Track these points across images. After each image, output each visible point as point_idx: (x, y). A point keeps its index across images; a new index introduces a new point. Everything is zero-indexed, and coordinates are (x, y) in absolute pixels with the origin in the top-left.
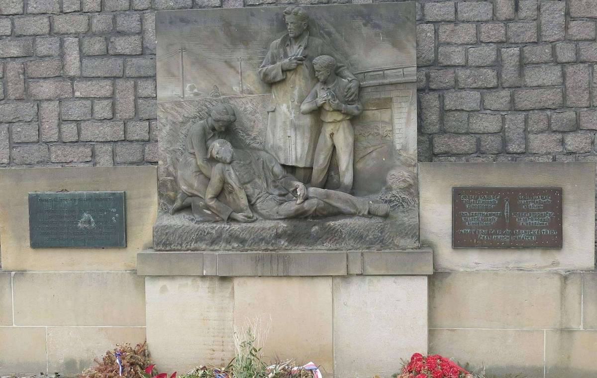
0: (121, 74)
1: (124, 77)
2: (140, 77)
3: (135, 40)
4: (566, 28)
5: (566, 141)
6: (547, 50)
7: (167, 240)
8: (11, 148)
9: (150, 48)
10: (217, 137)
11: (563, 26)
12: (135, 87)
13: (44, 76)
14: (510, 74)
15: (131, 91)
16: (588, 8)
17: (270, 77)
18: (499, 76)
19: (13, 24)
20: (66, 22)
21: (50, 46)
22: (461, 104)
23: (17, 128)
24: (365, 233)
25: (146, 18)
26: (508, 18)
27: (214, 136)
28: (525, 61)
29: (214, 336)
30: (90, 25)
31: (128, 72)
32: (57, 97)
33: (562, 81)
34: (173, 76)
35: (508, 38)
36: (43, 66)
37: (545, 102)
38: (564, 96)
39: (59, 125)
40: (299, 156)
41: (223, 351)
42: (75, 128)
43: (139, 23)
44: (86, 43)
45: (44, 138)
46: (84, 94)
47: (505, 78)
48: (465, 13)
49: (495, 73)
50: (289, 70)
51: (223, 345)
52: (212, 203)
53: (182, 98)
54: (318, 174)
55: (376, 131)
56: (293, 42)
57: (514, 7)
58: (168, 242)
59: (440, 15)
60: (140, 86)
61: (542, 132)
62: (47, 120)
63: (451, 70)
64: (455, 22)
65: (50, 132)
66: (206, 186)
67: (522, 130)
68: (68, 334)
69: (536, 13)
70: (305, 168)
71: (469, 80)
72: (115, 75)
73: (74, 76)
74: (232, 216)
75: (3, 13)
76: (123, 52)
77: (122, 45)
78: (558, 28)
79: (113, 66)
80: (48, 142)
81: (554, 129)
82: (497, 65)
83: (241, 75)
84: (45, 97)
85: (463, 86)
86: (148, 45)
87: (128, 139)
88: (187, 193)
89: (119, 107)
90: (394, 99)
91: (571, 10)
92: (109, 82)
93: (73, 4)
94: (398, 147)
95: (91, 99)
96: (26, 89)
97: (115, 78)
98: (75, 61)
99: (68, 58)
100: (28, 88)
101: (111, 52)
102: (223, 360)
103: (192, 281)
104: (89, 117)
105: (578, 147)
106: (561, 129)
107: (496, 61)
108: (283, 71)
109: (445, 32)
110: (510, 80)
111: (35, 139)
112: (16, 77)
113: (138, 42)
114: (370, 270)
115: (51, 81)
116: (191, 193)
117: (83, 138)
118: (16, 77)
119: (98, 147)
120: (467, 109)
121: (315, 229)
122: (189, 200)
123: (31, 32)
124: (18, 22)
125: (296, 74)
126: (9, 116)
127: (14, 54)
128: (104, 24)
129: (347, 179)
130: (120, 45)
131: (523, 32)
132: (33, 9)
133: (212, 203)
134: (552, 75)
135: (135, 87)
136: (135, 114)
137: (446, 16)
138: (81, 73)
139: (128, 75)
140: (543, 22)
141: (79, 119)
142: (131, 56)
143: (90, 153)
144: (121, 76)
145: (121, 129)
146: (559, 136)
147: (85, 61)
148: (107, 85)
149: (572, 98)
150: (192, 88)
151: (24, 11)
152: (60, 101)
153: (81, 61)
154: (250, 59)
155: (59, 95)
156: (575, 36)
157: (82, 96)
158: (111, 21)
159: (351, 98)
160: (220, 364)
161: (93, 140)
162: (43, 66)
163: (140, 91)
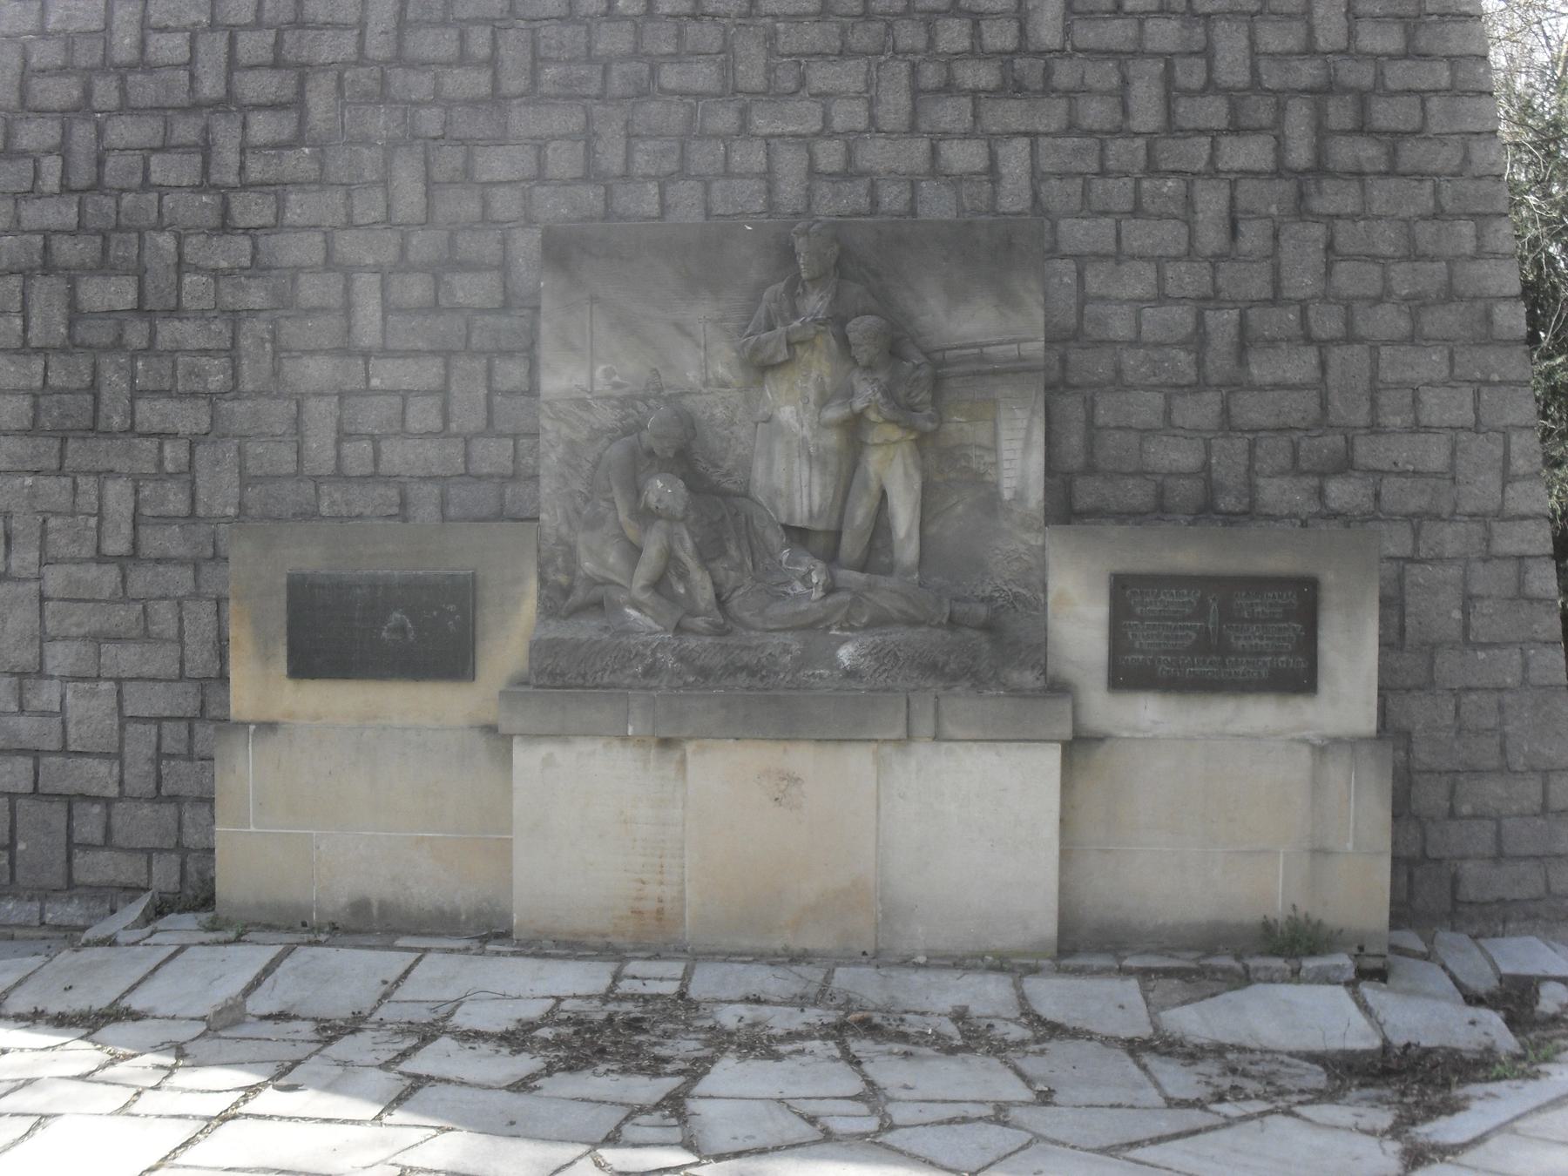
8: (243, 486)
18: (1200, 364)
35: (1217, 291)
36: (310, 329)
40: (816, 509)
41: (661, 883)
42: (370, 449)
51: (661, 873)
55: (964, 464)
82: (1198, 340)
101: (443, 302)
150: (609, 374)
152: (342, 396)
153: (384, 318)
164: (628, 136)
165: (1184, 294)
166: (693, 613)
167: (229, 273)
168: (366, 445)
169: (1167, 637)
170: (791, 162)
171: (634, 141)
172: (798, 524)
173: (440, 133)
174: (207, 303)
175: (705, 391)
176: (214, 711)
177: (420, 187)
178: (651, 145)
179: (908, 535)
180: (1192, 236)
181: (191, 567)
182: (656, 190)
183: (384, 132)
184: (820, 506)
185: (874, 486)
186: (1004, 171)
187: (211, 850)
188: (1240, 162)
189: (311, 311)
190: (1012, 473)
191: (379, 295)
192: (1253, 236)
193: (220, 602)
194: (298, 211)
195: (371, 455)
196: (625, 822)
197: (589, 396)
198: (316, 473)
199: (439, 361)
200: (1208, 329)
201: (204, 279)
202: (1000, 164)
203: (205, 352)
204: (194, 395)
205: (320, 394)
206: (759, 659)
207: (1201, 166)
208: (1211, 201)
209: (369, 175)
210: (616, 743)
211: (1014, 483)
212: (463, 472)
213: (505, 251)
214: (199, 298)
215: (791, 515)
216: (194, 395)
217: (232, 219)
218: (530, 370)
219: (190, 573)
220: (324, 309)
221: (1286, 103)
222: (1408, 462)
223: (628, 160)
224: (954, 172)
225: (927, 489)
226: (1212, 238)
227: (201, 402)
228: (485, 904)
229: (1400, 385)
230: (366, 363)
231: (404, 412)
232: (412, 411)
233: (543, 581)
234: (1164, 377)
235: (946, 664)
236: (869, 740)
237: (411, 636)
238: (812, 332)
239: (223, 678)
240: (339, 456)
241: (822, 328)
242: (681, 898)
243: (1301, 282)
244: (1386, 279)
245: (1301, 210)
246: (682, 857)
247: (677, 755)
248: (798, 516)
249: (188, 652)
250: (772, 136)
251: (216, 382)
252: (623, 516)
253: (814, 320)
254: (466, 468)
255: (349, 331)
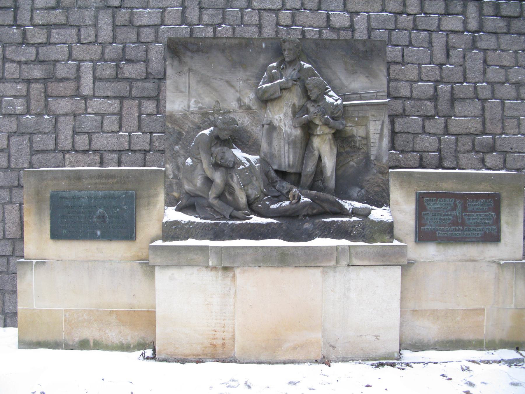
0: (127, 94)
1: (130, 97)
2: (144, 98)
3: (140, 67)
4: (485, 73)
5: (486, 160)
6: (470, 89)
7: (175, 234)
8: (32, 155)
9: (153, 74)
10: (219, 145)
11: (482, 71)
12: (140, 106)
13: (62, 95)
14: (443, 106)
15: (136, 109)
16: (499, 58)
17: (266, 96)
18: (436, 107)
19: (37, 51)
20: (83, 50)
21: (68, 70)
22: (408, 128)
23: (37, 138)
24: (350, 229)
25: (151, 49)
26: (442, 63)
27: (217, 143)
28: (455, 97)
29: (216, 319)
30: (103, 53)
31: (134, 93)
32: (72, 112)
33: (482, 113)
34: (181, 92)
35: (442, 78)
36: (61, 87)
37: (470, 129)
38: (484, 124)
39: (73, 137)
40: (291, 163)
41: (224, 332)
42: (87, 139)
43: (144, 53)
44: (99, 68)
45: (60, 147)
46: (96, 111)
47: (441, 109)
48: (410, 57)
49: (432, 105)
50: (285, 89)
51: (224, 327)
52: (215, 202)
53: (188, 111)
54: (306, 180)
55: (353, 144)
56: (288, 66)
57: (446, 54)
58: (176, 236)
59: (391, 57)
60: (144, 104)
61: (468, 152)
62: (63, 131)
63: (400, 101)
64: (403, 63)
65: (65, 142)
66: (210, 188)
67: (453, 150)
68: (83, 316)
69: (462, 60)
70: (295, 174)
71: (413, 109)
72: (122, 95)
73: (87, 95)
74: (232, 215)
75: (29, 42)
76: (130, 76)
77: (129, 71)
78: (478, 73)
79: (122, 88)
80: (63, 151)
81: (477, 150)
82: (435, 98)
83: (240, 93)
84: (62, 112)
85: (409, 114)
86: (151, 71)
87: (132, 149)
88: (191, 194)
89: (124, 122)
90: (371, 118)
91: (487, 60)
92: (117, 101)
93: (90, 36)
94: (372, 158)
95: (101, 115)
96: (46, 105)
97: (123, 97)
98: (89, 83)
99: (83, 81)
100: (48, 105)
101: (120, 76)
102: (224, 340)
103: (198, 270)
104: (99, 130)
105: (494, 164)
106: (482, 150)
107: (434, 96)
108: (281, 90)
109: (395, 71)
110: (444, 111)
111: (52, 147)
112: (38, 95)
113: (143, 69)
114: (356, 262)
115: (68, 99)
116: (195, 194)
117: (94, 147)
118: (38, 95)
119: (106, 156)
120: (413, 132)
121: (307, 226)
122: (192, 200)
123: (53, 58)
124: (42, 50)
125: (290, 93)
126: (31, 128)
127: (37, 76)
128: (115, 53)
129: (332, 183)
130: (128, 70)
131: (452, 74)
132: (55, 39)
133: (215, 202)
134: (475, 108)
135: (140, 106)
136: (139, 127)
137: (395, 59)
138: (94, 93)
139: (133, 96)
140: (467, 67)
141: (90, 131)
142: (137, 80)
143: (99, 160)
144: (128, 96)
145: (126, 140)
146: (481, 155)
147: (97, 83)
148: (115, 103)
149: (489, 127)
150: (196, 102)
151: (47, 41)
152: (75, 116)
153: (94, 83)
154: (247, 80)
155: (74, 110)
156: (491, 79)
157: (93, 112)
158: (121, 51)
159: (338, 114)
160: (221, 343)
161: (102, 149)
162: (61, 87)
163: (143, 109)
164: (201, 8)
165: (429, 79)
166: (238, 209)
167: (26, 63)
168: (86, 137)
169: (440, 219)
170: (269, 19)
171: (202, 10)
172: (283, 169)
173: (119, 5)
174: (17, 76)
175: (240, 111)
176: (17, 253)
177: (110, 27)
178: (211, 11)
179: (332, 175)
180: (432, 55)
181: (8, 190)
182: (212, 30)
183: (95, 4)
184: (293, 161)
185: (316, 153)
186: (356, 27)
187: (16, 313)
188: (450, 27)
189: (61, 80)
190: (375, 149)
191: (92, 73)
192: (456, 55)
193: (21, 205)
194: (57, 37)
195: (88, 141)
196: (207, 305)
197: (188, 113)
198: (63, 149)
199: (117, 101)
200: (438, 93)
201: (15, 65)
202: (355, 25)
203: (15, 97)
204: (10, 115)
205: (66, 115)
206: (268, 230)
207: (434, 28)
208: (439, 40)
209: (89, 22)
210: (204, 269)
211: (375, 152)
212: (128, 149)
213: (147, 55)
214: (12, 74)
215: (280, 165)
216: (10, 115)
217: (27, 40)
218: (157, 105)
219: (8, 193)
220: (68, 79)
221: (467, 4)
222: (516, 148)
223: (200, 18)
224: (336, 27)
225: (339, 154)
226: (440, 56)
227: (14, 118)
228: (141, 340)
229: (513, 117)
230: (86, 102)
231: (102, 123)
232: (106, 122)
233: (167, 194)
234: (422, 112)
235: (352, 231)
236: (319, 266)
237: (108, 220)
238: (290, 84)
239: (22, 238)
240: (73, 142)
241: (295, 83)
242: (233, 338)
243: (474, 74)
244: (507, 75)
245: (474, 45)
246: (234, 320)
247: (231, 274)
248: (283, 166)
249: (7, 227)
250: (261, 9)
251: (19, 109)
252: (205, 165)
253: (292, 79)
254: (129, 147)
255: (78, 88)
